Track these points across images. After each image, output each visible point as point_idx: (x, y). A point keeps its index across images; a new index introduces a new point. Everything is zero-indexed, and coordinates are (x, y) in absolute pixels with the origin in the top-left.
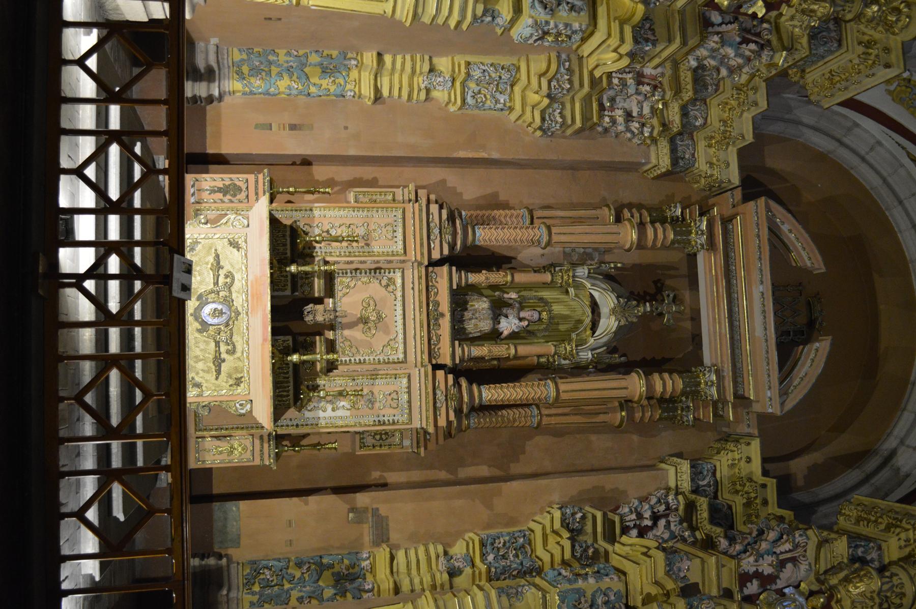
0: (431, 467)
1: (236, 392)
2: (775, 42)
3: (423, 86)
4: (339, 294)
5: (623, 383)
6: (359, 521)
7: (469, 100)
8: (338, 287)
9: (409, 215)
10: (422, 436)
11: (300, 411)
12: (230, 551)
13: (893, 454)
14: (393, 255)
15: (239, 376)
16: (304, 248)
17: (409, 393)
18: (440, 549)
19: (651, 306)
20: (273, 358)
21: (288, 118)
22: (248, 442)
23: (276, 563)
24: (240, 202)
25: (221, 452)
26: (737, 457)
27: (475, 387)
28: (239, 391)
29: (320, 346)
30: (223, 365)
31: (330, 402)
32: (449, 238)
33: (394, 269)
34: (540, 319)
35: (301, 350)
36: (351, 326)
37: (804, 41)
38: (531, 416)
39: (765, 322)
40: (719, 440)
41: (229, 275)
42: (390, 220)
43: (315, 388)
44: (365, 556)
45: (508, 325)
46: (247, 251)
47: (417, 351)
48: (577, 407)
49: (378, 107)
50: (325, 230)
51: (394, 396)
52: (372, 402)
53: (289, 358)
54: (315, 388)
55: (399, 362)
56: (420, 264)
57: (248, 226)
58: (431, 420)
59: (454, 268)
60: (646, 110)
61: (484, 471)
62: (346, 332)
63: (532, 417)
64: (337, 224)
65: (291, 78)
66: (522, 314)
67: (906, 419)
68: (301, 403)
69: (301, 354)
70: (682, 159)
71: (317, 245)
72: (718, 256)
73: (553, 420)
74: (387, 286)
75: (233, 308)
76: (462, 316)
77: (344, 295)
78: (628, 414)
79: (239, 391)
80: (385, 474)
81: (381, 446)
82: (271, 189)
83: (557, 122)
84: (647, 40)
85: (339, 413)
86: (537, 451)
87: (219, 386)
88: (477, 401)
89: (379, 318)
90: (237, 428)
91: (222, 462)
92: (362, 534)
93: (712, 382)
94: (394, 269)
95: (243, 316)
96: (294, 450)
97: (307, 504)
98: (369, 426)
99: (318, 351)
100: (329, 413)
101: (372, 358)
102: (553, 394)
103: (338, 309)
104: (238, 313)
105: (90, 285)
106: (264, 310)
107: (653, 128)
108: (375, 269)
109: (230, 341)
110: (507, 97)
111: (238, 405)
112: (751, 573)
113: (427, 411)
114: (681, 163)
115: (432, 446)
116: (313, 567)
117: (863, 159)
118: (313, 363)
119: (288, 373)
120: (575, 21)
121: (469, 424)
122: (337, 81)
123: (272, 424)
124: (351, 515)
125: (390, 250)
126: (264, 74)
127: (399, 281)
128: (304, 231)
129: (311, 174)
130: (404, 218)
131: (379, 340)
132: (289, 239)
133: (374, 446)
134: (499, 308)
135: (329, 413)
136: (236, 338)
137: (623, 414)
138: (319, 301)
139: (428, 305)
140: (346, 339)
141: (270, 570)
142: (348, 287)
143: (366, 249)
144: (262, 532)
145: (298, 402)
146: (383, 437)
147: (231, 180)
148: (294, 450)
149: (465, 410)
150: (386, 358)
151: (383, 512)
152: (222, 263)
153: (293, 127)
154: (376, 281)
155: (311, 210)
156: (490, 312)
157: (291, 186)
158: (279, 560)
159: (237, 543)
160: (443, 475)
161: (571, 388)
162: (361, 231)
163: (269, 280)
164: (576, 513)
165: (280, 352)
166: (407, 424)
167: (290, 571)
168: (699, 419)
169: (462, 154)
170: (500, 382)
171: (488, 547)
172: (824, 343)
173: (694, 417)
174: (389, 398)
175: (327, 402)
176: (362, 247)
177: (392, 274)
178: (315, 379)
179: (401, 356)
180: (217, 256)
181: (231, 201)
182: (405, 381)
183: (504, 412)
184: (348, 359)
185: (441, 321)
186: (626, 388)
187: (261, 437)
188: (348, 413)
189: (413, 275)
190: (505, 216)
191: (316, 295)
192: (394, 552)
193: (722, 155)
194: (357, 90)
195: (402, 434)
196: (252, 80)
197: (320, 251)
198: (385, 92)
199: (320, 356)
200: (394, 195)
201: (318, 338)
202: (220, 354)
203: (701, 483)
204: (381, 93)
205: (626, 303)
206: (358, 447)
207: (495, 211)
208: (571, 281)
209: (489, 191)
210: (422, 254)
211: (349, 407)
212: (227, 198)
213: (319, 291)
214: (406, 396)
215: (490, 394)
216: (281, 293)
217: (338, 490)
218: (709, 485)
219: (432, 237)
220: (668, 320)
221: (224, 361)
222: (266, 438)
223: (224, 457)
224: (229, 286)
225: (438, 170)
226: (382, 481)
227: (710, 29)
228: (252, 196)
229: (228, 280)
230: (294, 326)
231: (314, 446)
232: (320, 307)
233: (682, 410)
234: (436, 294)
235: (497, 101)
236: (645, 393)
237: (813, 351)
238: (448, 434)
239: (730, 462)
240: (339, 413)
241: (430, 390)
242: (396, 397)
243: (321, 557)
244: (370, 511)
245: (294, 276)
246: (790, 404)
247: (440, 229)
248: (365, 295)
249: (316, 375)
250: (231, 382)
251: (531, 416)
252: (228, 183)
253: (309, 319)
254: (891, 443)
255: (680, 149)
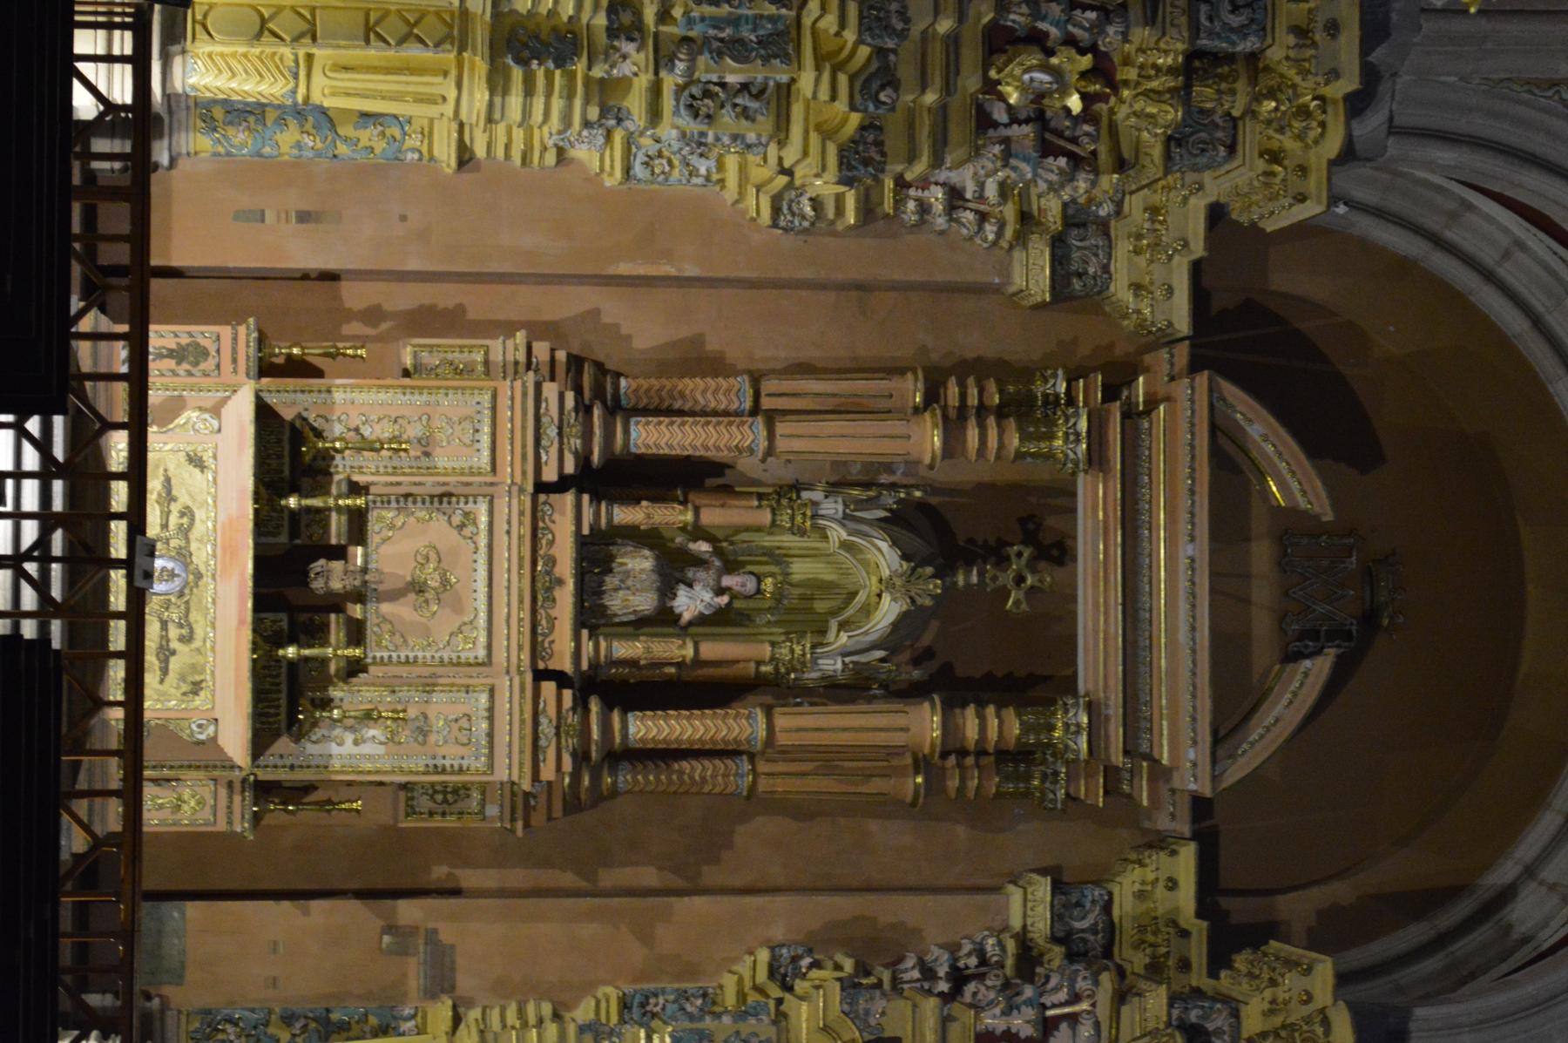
0: (547, 863)
1: (192, 705)
2: (1104, 156)
3: (550, 143)
4: (374, 539)
5: (901, 720)
6: (402, 950)
7: (639, 170)
8: (373, 526)
9: (504, 402)
10: (521, 803)
11: (297, 740)
12: (167, 990)
13: (1506, 895)
14: (472, 474)
15: (198, 678)
16: (314, 458)
17: (491, 719)
18: (547, 1009)
19: (981, 574)
20: (254, 651)
21: (295, 200)
22: (207, 792)
23: (247, 1014)
24: (206, 375)
25: (161, 807)
26: (1151, 877)
27: (616, 717)
28: (197, 703)
29: (336, 632)
30: (173, 659)
31: (351, 729)
32: (576, 443)
33: (475, 496)
34: (759, 591)
35: (302, 637)
36: (394, 596)
37: (1157, 152)
38: (736, 774)
39: (1194, 617)
40: (1136, 848)
41: (187, 512)
42: (470, 411)
43: (326, 704)
44: (407, 1011)
45: (691, 602)
46: (215, 472)
47: (511, 648)
48: (827, 758)
49: (466, 177)
50: (352, 426)
51: (464, 723)
52: (423, 732)
53: (281, 652)
54: (326, 704)
55: (478, 664)
56: (521, 490)
57: (219, 430)
58: (528, 769)
59: (586, 498)
60: (991, 191)
61: (649, 876)
62: (386, 608)
63: (738, 777)
64: (374, 417)
65: (302, 126)
66: (727, 581)
67: (1546, 825)
68: (300, 729)
69: (301, 646)
70: (1080, 275)
71: (338, 457)
72: (1111, 484)
73: (780, 786)
74: (461, 527)
75: (192, 567)
76: (601, 583)
77: (384, 541)
78: (926, 780)
79: (197, 703)
80: (458, 872)
81: (444, 814)
82: (260, 350)
83: (804, 217)
84: (867, 162)
85: (367, 749)
86: (756, 840)
87: (165, 694)
88: (618, 740)
89: (445, 582)
90: (190, 767)
91: (162, 822)
92: (405, 975)
93: (1078, 725)
94: (475, 496)
95: (207, 579)
96: (286, 811)
97: (306, 913)
98: (417, 773)
99: (333, 639)
100: (348, 747)
101: (428, 655)
102: (762, 732)
103: (372, 566)
104: (199, 576)
105: (31, 568)
106: (242, 574)
107: (1002, 225)
108: (441, 496)
109: (185, 623)
110: (712, 163)
111: (194, 727)
112: (998, 1032)
113: (521, 752)
114: (1077, 284)
115: (538, 819)
116: (313, 1025)
117: (1489, 276)
118: (324, 662)
119: (278, 676)
120: (749, 130)
121: (614, 783)
122: (388, 132)
123: (249, 759)
124: (386, 939)
125: (466, 465)
126: (251, 119)
127: (483, 519)
128: (314, 429)
129: (337, 297)
130: (494, 409)
131: (443, 622)
132: (287, 446)
133: (431, 814)
134: (674, 567)
135: (348, 747)
136: (194, 616)
137: (919, 780)
138: (339, 553)
139: (534, 563)
140: (385, 620)
141: (236, 1025)
142: (392, 527)
143: (425, 462)
144: (223, 953)
145: (297, 730)
146: (450, 795)
147: (190, 334)
148: (286, 811)
149: (594, 754)
150: (454, 656)
151: (447, 934)
152: (174, 492)
153: (304, 217)
154: (441, 517)
155: (329, 391)
156: (654, 577)
157: (295, 345)
158: (253, 1010)
159: (178, 977)
160: (568, 879)
161: (797, 724)
162: (414, 431)
163: (250, 525)
164: (800, 957)
165: (266, 640)
166: (484, 773)
167: (271, 1030)
168: (1075, 799)
169: (624, 269)
170: (701, 706)
171: (635, 1010)
172: (1319, 660)
173: (1067, 794)
174: (455, 727)
175: (346, 728)
176: (417, 458)
177: (471, 505)
178: (325, 688)
179: (481, 653)
180: (168, 480)
181: (190, 374)
182: (484, 699)
183: (685, 764)
184: (386, 655)
185: (557, 593)
186: (906, 730)
187: (230, 785)
188: (381, 750)
189: (512, 509)
190: (704, 392)
191: (334, 541)
192: (461, 1010)
193: (1158, 272)
194: (425, 149)
195: (483, 793)
196: (231, 131)
197: (343, 468)
198: (480, 151)
199: (335, 650)
200: (486, 353)
201: (333, 617)
202: (168, 641)
203: (1077, 925)
204: (472, 152)
205: (914, 570)
206: (402, 814)
207: (687, 380)
208: (808, 523)
209: (684, 332)
210: (524, 473)
211: (383, 739)
212: (181, 370)
213: (339, 535)
214: (485, 725)
215: (643, 728)
216: (271, 540)
217: (361, 894)
218: (1093, 929)
219: (544, 443)
220: (1017, 603)
221: (173, 653)
222: (237, 786)
223: (166, 814)
224: (185, 532)
225: (584, 290)
226: (450, 885)
227: (991, 133)
228: (227, 366)
229: (185, 520)
230: (292, 594)
231: (319, 804)
232: (337, 565)
233: (1044, 777)
234: (551, 543)
235: (693, 173)
236: (939, 742)
237: (1299, 677)
238: (573, 804)
239: (1137, 887)
240: (367, 749)
241: (528, 715)
242: (466, 725)
243: (328, 1011)
244: (422, 931)
245: (294, 515)
246: (1235, 773)
247: (560, 428)
248: (420, 543)
249: (327, 681)
250: (185, 688)
251: (736, 774)
252: (185, 340)
253: (317, 585)
254: (1505, 873)
255: (1076, 255)
